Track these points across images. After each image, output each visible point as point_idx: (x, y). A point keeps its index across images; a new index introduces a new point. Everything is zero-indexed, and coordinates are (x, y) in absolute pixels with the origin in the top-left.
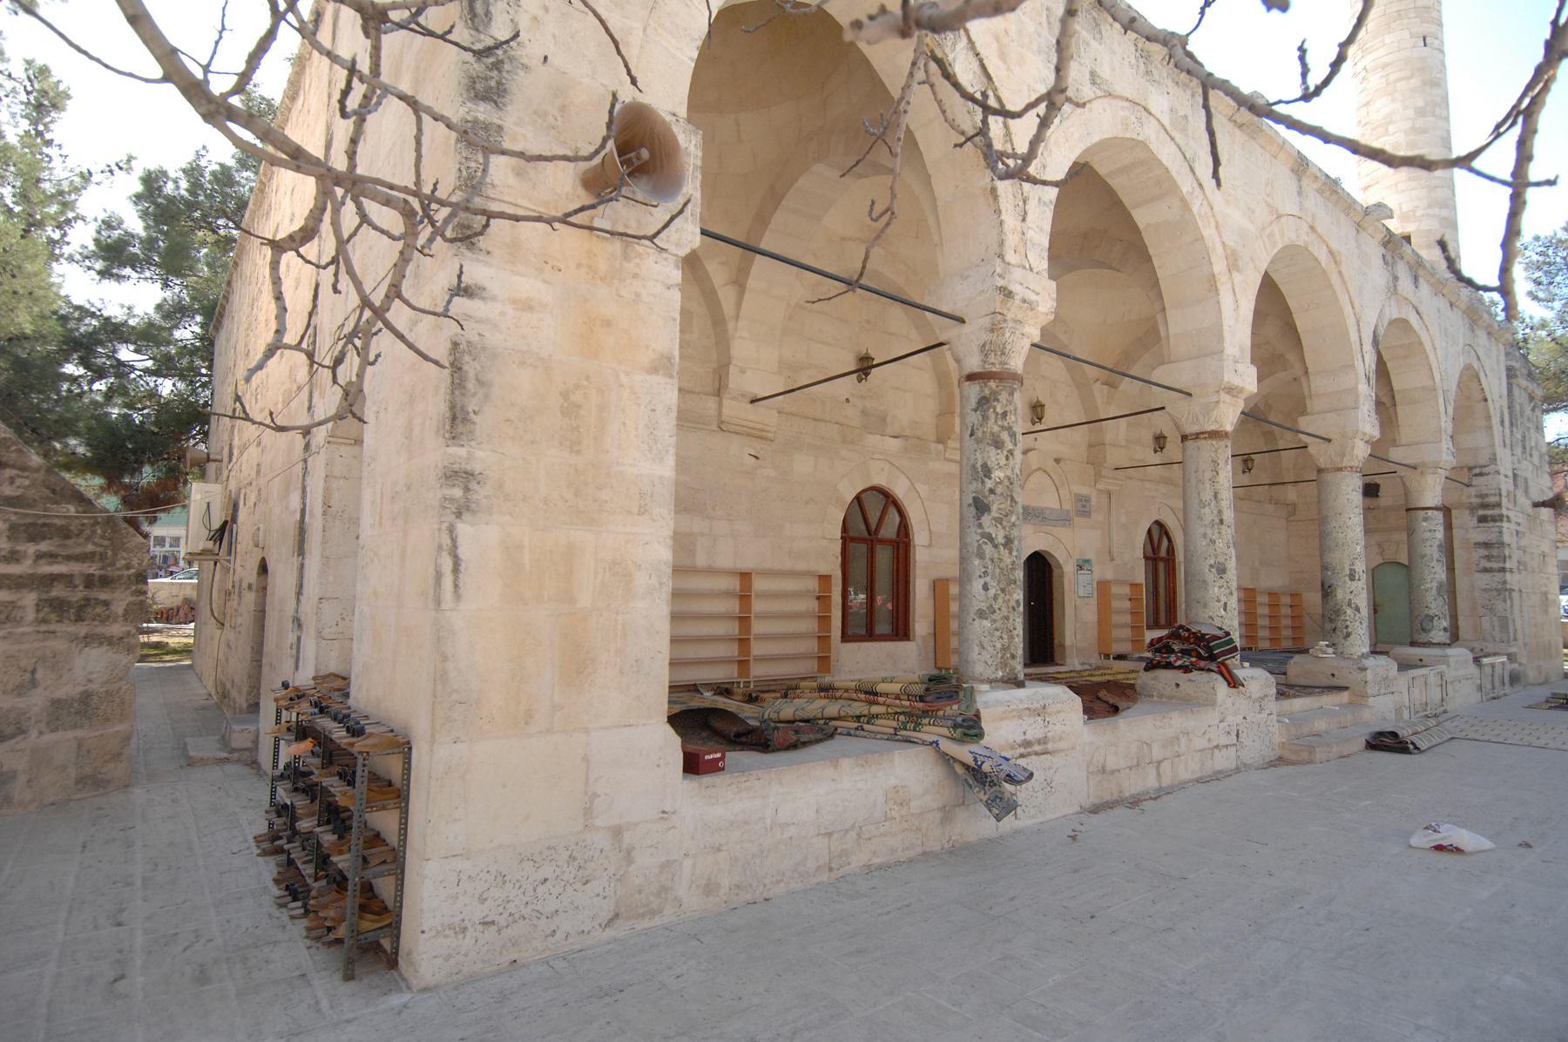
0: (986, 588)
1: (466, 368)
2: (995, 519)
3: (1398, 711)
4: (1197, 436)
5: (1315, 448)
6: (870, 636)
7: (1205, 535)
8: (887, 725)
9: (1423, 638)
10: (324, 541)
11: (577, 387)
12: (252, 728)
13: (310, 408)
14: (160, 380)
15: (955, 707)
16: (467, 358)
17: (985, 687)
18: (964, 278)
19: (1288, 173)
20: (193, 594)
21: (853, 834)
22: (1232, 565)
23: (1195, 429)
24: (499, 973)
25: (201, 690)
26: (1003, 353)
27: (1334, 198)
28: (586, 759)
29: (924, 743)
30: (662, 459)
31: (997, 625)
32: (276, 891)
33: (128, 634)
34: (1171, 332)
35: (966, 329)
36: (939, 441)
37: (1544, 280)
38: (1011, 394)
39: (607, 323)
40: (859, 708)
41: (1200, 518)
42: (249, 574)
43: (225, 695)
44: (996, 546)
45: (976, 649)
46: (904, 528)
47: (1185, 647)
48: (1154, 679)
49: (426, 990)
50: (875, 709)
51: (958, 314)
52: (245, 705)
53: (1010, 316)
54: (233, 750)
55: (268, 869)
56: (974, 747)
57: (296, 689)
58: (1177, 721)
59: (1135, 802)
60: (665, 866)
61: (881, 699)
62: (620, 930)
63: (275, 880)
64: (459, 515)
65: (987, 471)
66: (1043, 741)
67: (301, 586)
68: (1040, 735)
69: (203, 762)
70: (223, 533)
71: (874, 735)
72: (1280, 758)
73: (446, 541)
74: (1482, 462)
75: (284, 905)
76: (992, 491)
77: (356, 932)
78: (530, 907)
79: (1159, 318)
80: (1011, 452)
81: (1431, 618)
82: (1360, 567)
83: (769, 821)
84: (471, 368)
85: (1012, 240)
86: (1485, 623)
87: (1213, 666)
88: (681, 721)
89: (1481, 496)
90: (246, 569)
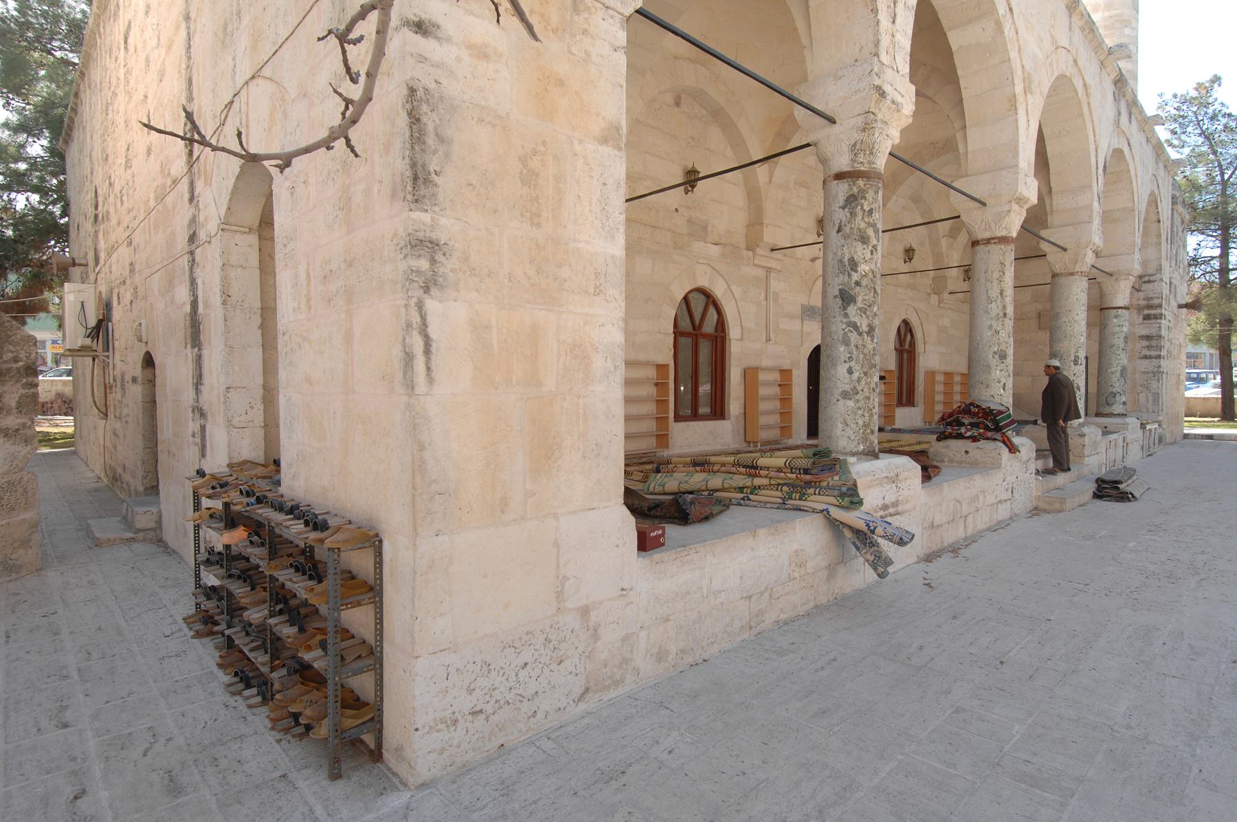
0: (850, 371)
1: (424, 119)
2: (860, 309)
3: (1100, 467)
4: (988, 241)
5: (1053, 255)
6: (695, 416)
7: (990, 327)
8: (775, 495)
9: (1107, 410)
10: (227, 330)
11: (535, 152)
12: (155, 510)
13: (191, 199)
14: (13, 195)
15: (837, 478)
16: (425, 108)
17: (852, 460)
18: (838, 78)
19: (1064, 7)
20: (68, 391)
21: (766, 595)
22: (1010, 352)
23: (987, 235)
24: (489, 761)
25: (92, 469)
26: (871, 153)
27: (1091, 36)
28: (556, 544)
29: (814, 511)
30: (613, 237)
31: (861, 404)
32: (225, 678)
33: (24, 425)
34: (970, 149)
35: (836, 129)
36: (749, 249)
37: (1178, 130)
38: (876, 193)
39: (560, 83)
40: (740, 480)
41: (987, 312)
42: (134, 367)
43: (115, 478)
44: (860, 334)
45: (840, 426)
46: (721, 324)
47: (975, 420)
48: (947, 447)
49: (423, 786)
50: (757, 481)
51: (829, 113)
52: (141, 488)
53: (880, 116)
54: (138, 531)
55: (206, 653)
56: (856, 513)
57: (213, 477)
58: (979, 482)
59: (954, 550)
60: (625, 639)
61: (763, 473)
62: (590, 704)
63: (220, 666)
64: (427, 290)
65: (854, 265)
66: (895, 504)
67: (200, 376)
68: (894, 500)
69: (110, 543)
70: (101, 329)
71: (764, 505)
72: (1036, 508)
73: (416, 319)
74: (1150, 271)
75: (239, 693)
76: (858, 284)
77: (338, 730)
78: (513, 691)
79: (959, 136)
80: (875, 247)
81: (1114, 395)
82: (1082, 354)
83: (705, 591)
84: (430, 121)
85: (885, 41)
86: (1142, 398)
87: (998, 436)
88: (635, 503)
89: (1148, 299)
90: (126, 361)
